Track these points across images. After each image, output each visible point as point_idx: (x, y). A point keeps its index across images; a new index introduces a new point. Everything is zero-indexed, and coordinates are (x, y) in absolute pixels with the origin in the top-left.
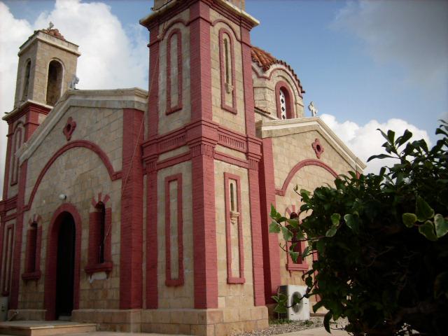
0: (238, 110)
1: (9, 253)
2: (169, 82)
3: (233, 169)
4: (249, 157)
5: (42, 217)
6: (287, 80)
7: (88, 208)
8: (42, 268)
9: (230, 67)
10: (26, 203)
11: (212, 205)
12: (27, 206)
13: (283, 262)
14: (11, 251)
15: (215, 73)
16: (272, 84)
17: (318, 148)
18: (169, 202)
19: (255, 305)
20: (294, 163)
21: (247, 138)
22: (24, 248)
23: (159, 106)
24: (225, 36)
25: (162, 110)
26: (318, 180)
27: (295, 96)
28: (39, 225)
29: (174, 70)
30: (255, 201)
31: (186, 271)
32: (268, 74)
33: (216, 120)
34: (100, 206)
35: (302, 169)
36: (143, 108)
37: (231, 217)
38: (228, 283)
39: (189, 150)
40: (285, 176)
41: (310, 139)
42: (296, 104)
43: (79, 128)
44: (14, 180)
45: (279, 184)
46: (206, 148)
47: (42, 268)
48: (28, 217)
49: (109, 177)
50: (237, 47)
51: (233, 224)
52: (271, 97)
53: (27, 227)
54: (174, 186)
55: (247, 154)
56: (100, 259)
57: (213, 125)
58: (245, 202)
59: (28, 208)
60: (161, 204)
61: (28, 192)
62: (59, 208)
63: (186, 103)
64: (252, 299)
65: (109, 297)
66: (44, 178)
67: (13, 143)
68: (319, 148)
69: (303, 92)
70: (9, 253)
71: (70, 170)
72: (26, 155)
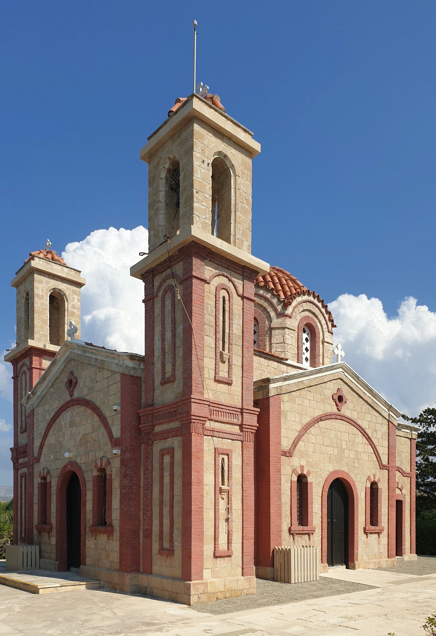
0: (234, 379)
1: (23, 501)
2: (163, 349)
3: (225, 444)
4: (244, 430)
5: (51, 471)
6: (314, 314)
7: (92, 470)
8: (53, 521)
9: (227, 331)
10: (36, 454)
11: (201, 482)
12: (36, 459)
13: (285, 526)
14: (25, 500)
15: (210, 341)
16: (292, 323)
17: (340, 399)
18: (163, 475)
19: (243, 575)
20: (307, 420)
21: (242, 409)
22: (36, 499)
23: (155, 373)
24: (223, 293)
25: (158, 379)
26: (336, 436)
27: (323, 332)
28: (48, 480)
29: (168, 335)
30: (249, 474)
31: (176, 544)
32: (289, 311)
33: (208, 395)
34: (102, 470)
35: (316, 425)
36: (138, 373)
37: (220, 493)
38: (215, 557)
39: (180, 425)
40: (294, 435)
41: (331, 389)
42: (323, 342)
43: (81, 384)
44: (24, 426)
45: (286, 444)
46: (195, 426)
47: (53, 521)
48: (38, 469)
49: (109, 443)
50: (237, 302)
51: (223, 499)
52: (291, 338)
53: (37, 480)
54: (167, 459)
55: (241, 426)
56: (102, 522)
57: (202, 402)
58: (237, 475)
59: (38, 460)
60: (156, 474)
61: (37, 443)
62: (65, 466)
63: (179, 374)
64: (240, 569)
65: (111, 559)
66: (51, 432)
67: (19, 387)
68: (340, 399)
69: (333, 326)
70: (23, 501)
71: (74, 428)
72: (32, 405)
